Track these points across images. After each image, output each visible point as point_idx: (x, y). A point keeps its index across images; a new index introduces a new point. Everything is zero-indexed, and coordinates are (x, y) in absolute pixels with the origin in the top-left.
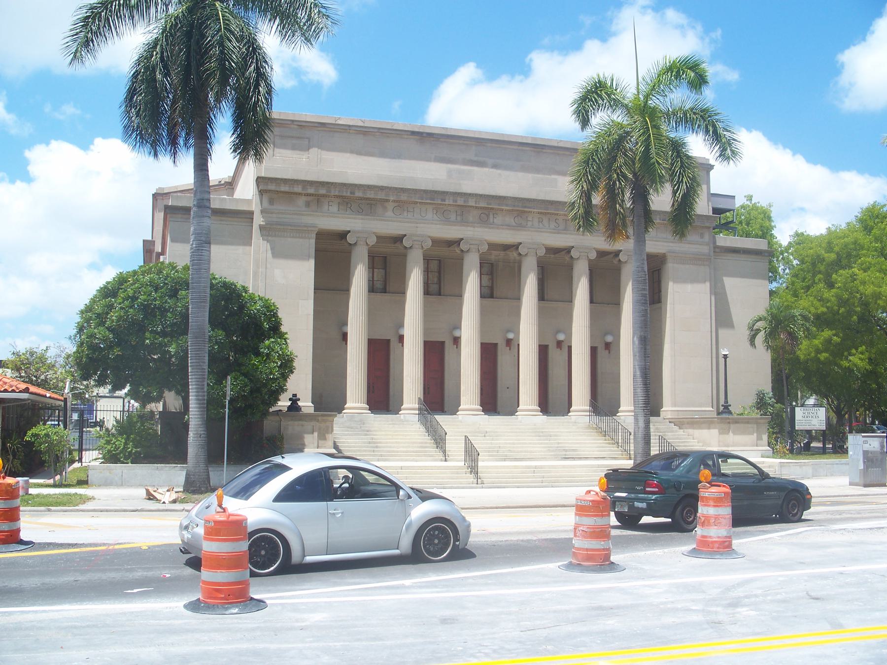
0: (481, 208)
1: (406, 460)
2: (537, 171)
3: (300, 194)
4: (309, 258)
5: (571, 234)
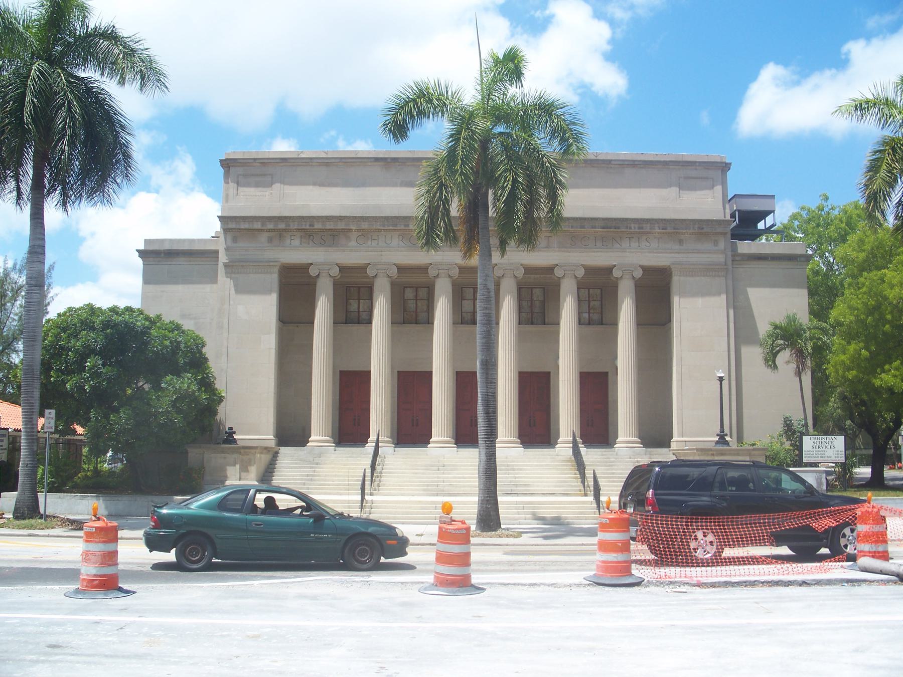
0: (269, 230)
1: (330, 494)
3: (262, 230)
4: (269, 292)
5: (555, 251)
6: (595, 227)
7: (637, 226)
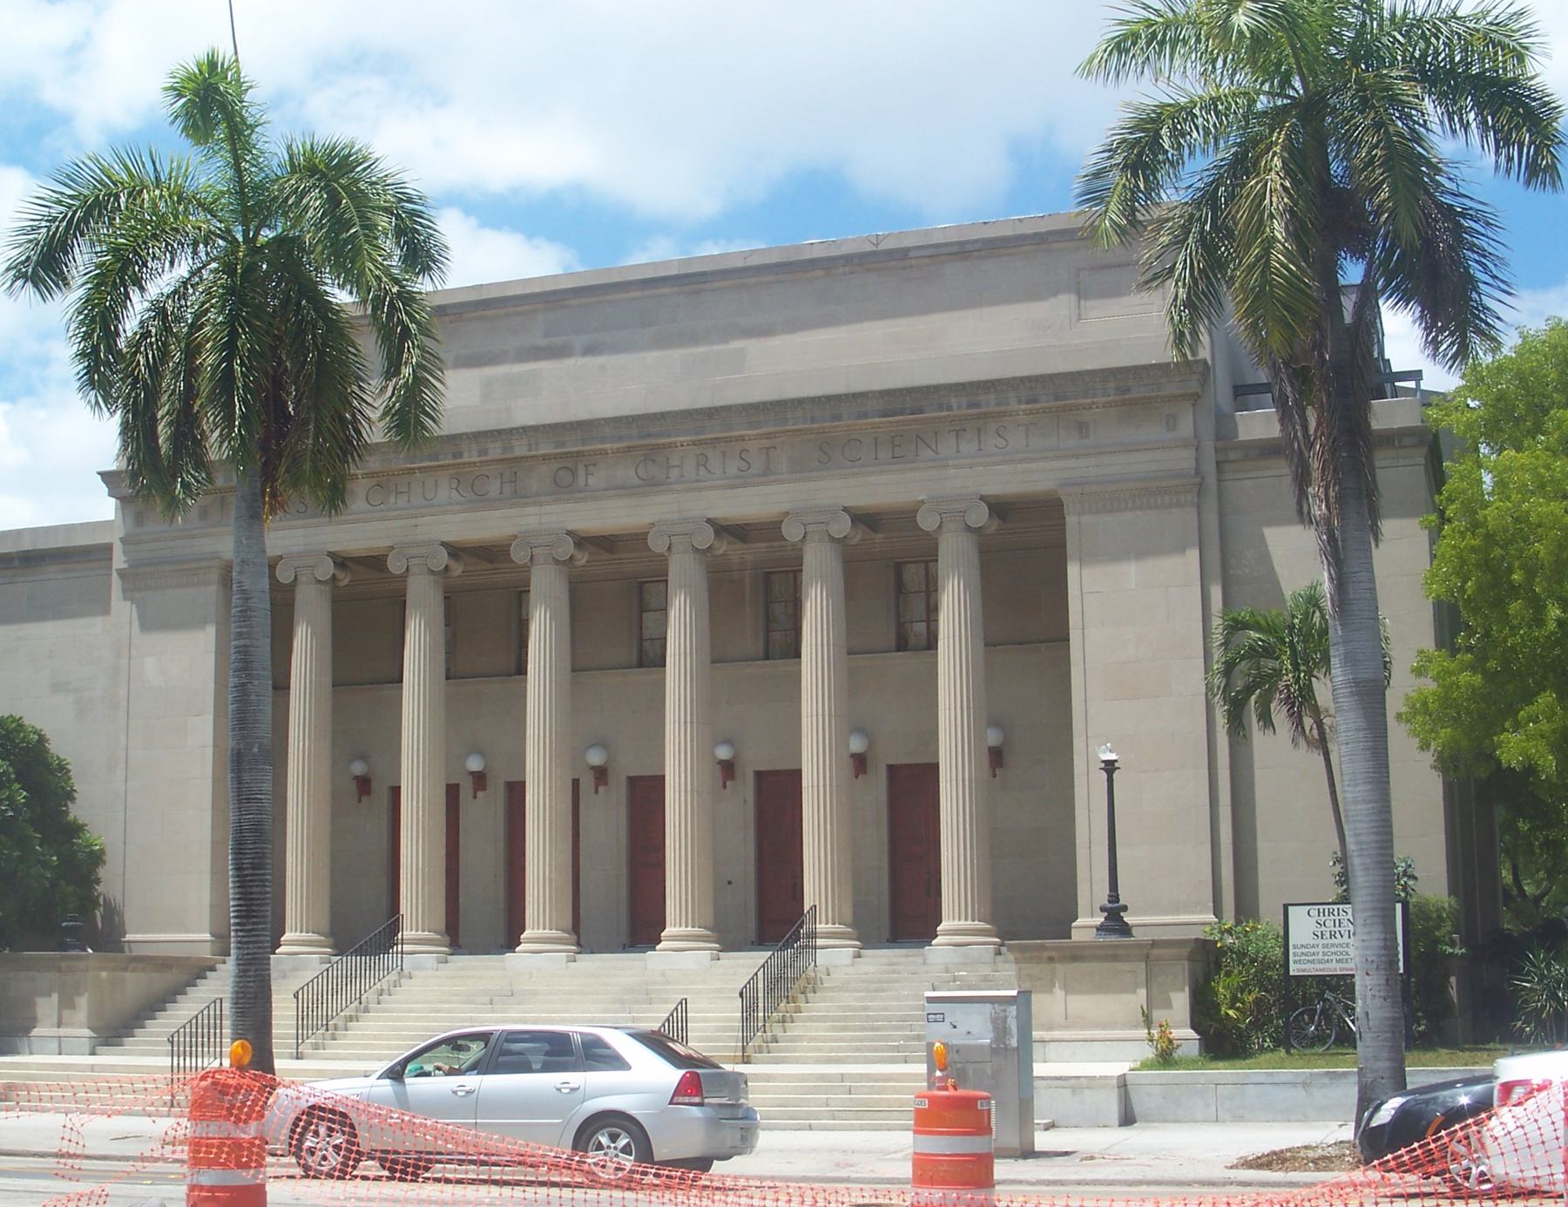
2: (693, 338)
4: (200, 624)
5: (782, 482)
6: (865, 415)
7: (964, 401)
